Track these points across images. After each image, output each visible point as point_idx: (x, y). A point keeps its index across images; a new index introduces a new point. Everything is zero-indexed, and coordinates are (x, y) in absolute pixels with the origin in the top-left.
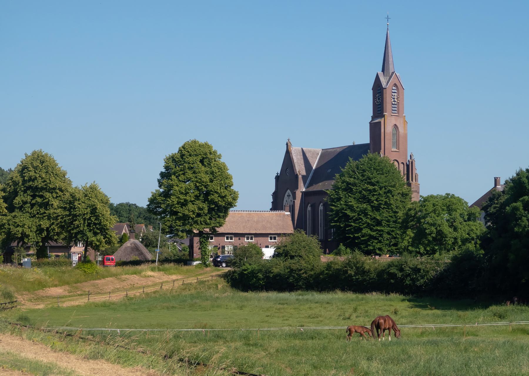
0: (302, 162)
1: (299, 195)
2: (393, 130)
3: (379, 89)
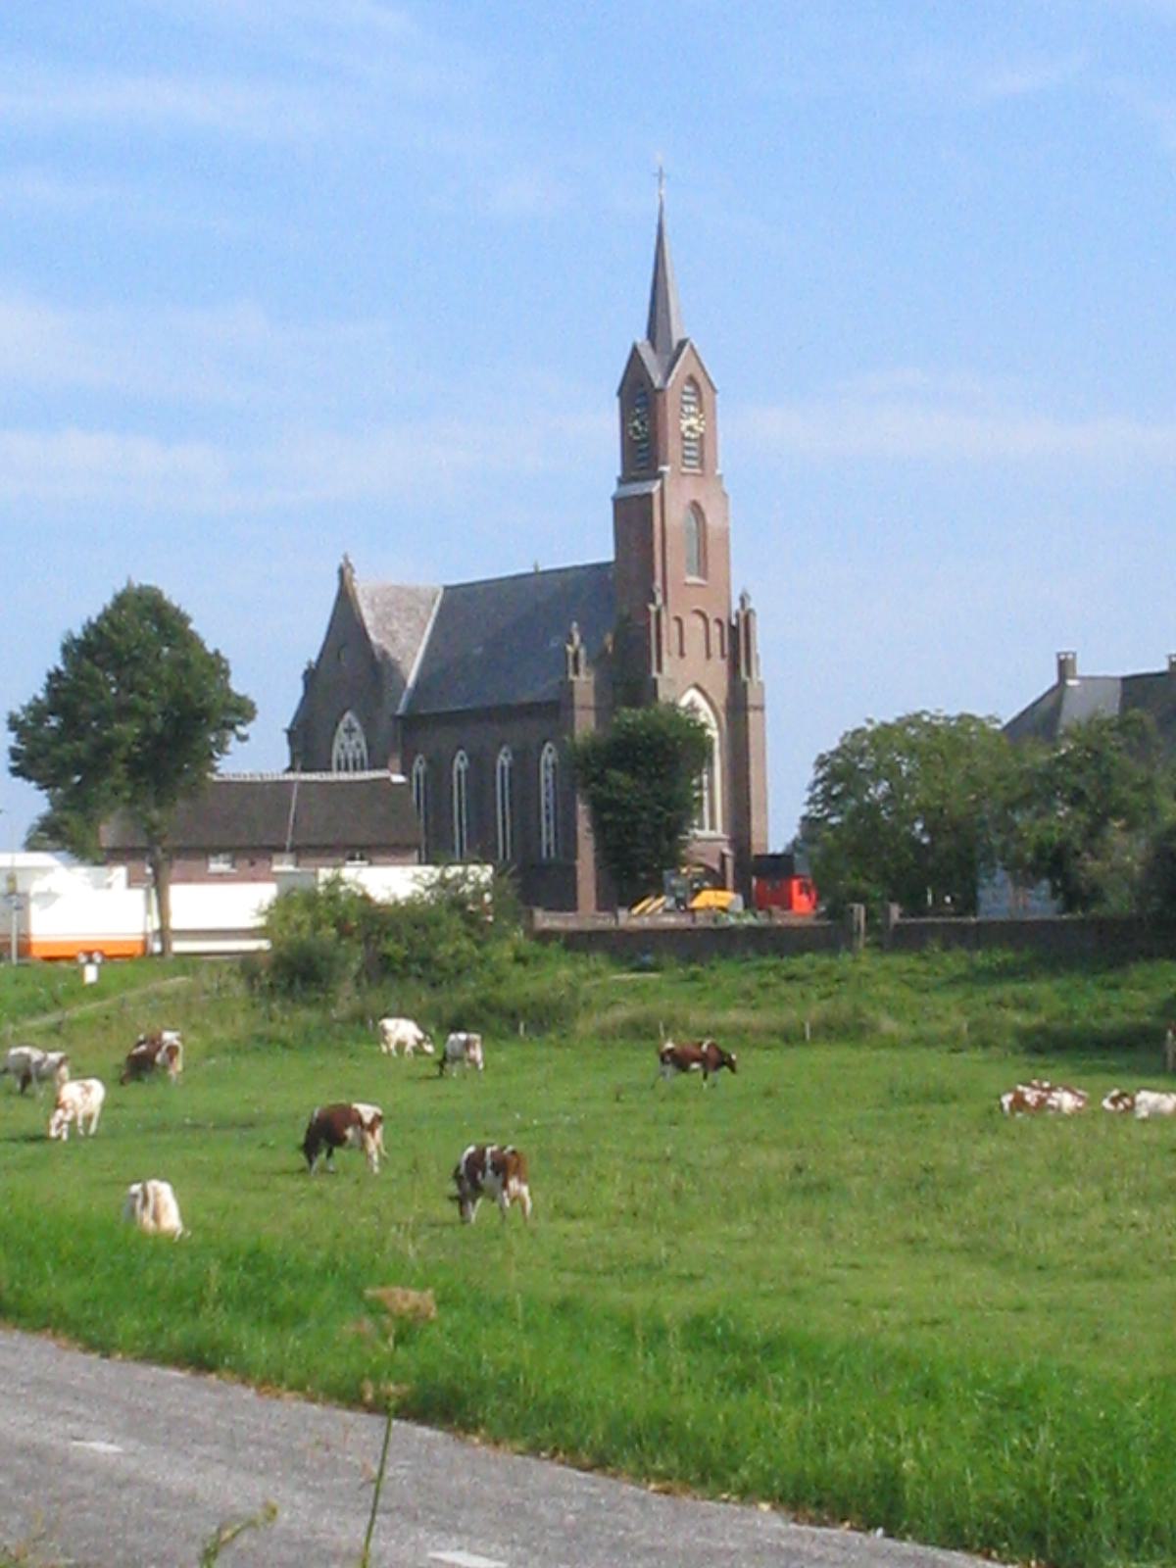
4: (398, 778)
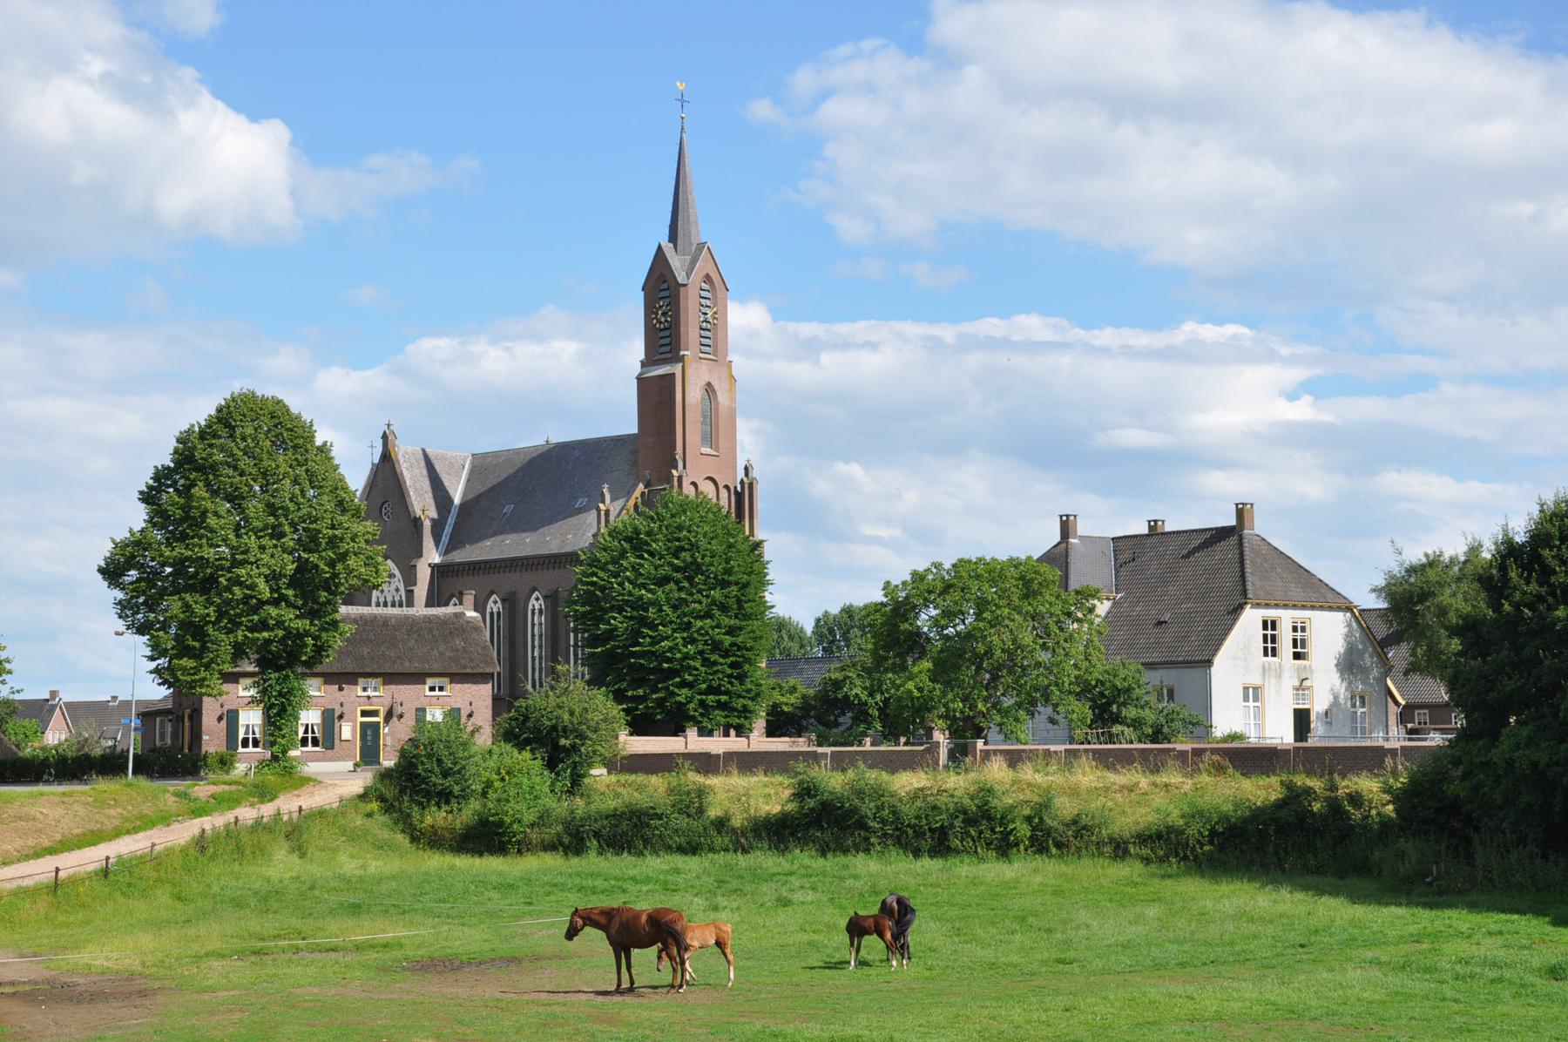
0: (426, 484)
1: (424, 574)
3: (665, 286)
4: (471, 614)
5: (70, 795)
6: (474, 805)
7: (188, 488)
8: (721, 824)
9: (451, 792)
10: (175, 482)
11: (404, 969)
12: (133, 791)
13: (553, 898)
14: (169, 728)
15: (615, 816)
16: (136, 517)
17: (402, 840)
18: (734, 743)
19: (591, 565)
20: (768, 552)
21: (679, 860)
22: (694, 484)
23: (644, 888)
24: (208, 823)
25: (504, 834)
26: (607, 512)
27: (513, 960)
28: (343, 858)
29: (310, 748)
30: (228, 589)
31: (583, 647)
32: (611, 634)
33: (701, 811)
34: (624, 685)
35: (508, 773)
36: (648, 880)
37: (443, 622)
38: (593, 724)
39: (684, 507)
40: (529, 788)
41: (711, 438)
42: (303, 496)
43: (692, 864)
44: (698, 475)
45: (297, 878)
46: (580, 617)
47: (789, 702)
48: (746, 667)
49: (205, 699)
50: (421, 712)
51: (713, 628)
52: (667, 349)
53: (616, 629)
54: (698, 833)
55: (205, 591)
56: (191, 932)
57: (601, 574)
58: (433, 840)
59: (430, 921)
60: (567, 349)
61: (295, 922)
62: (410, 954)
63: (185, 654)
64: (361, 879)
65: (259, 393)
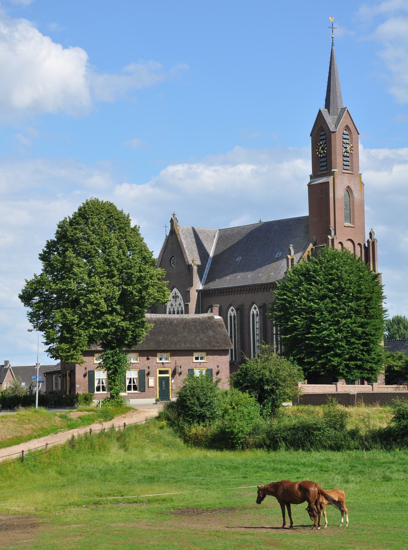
0: (194, 247)
1: (194, 296)
2: (345, 196)
3: (323, 133)
4: (217, 317)
5: (6, 417)
6: (218, 423)
7: (64, 251)
8: (354, 434)
9: (205, 415)
10: (58, 249)
11: (171, 513)
12: (37, 414)
13: (258, 474)
14: (59, 380)
15: (294, 429)
16: (37, 268)
17: (179, 441)
18: (366, 388)
19: (283, 290)
20: (384, 280)
21: (330, 454)
22: (341, 243)
23: (309, 470)
24: (77, 432)
25: (234, 438)
26: (292, 260)
27: (232, 509)
28: (147, 451)
29: (132, 391)
30: (85, 306)
31: (281, 334)
32: (294, 328)
33: (342, 426)
34: (302, 356)
35: (237, 405)
36: (312, 465)
37: (202, 322)
38: (282, 377)
39: (334, 256)
40: (247, 414)
41: (350, 217)
42: (124, 255)
43: (337, 456)
44: (343, 238)
45: (123, 462)
46: (277, 318)
47: (397, 365)
48: (371, 345)
49: (77, 365)
50: (191, 372)
51: (352, 323)
52: (325, 168)
53: (297, 325)
54: (340, 439)
55: (73, 307)
56: (63, 492)
57: (289, 294)
58: (196, 442)
59: (189, 487)
60: (246, 169)
61: (119, 487)
62: (176, 504)
63: (64, 342)
64: (156, 463)
65: (100, 200)
